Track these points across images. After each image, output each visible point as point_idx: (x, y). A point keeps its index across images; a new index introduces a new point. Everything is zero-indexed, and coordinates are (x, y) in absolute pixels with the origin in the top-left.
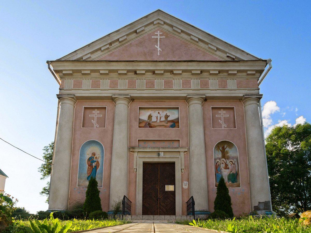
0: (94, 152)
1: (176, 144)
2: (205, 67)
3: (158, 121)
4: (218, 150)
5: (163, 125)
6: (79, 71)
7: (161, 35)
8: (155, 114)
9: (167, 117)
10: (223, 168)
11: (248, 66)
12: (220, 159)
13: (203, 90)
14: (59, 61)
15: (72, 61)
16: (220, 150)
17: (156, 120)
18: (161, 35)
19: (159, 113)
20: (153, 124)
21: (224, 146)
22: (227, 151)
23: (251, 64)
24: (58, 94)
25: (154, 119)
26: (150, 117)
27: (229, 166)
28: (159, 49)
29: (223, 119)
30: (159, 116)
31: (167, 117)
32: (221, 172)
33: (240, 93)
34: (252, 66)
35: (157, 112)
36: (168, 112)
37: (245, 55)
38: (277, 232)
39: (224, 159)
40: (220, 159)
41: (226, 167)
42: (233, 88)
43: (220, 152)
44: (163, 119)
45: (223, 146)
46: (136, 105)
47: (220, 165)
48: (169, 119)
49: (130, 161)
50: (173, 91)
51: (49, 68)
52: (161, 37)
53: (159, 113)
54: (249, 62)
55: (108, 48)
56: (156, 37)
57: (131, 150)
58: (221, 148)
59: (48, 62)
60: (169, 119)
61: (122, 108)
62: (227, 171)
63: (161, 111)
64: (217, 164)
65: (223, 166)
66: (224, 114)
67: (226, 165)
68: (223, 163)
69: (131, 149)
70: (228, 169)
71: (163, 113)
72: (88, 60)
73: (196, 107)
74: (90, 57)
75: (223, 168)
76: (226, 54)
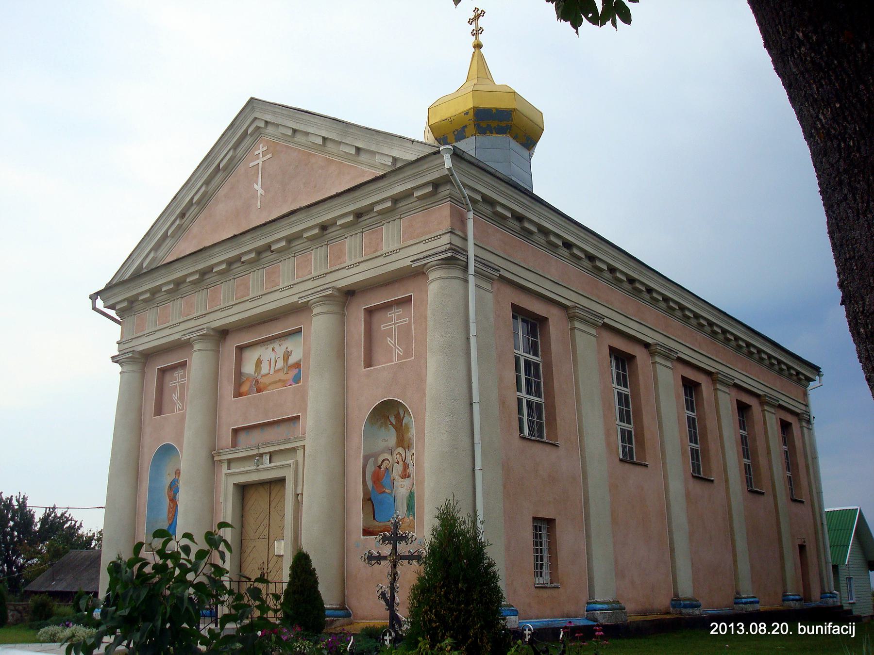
0: (538, 451)
2: (325, 216)
3: (272, 372)
4: (386, 426)
5: (280, 380)
8: (266, 354)
9: (287, 355)
10: (397, 478)
11: (404, 180)
12: (391, 451)
13: (338, 270)
14: (109, 287)
16: (392, 424)
18: (265, 153)
19: (273, 350)
21: (399, 413)
23: (414, 171)
25: (265, 369)
26: (259, 362)
27: (412, 470)
28: (261, 191)
29: (395, 335)
30: (273, 355)
31: (287, 355)
32: (392, 487)
33: (403, 261)
35: (270, 347)
36: (289, 344)
37: (409, 145)
39: (400, 450)
40: (391, 451)
41: (405, 475)
43: (393, 431)
44: (280, 364)
45: (388, 413)
46: (230, 347)
47: (390, 470)
48: (292, 360)
53: (273, 350)
54: (405, 169)
58: (393, 419)
59: (483, 12)
61: (198, 361)
62: (407, 482)
63: (276, 345)
64: (380, 467)
65: (398, 469)
67: (406, 466)
68: (398, 463)
69: (213, 461)
70: (409, 477)
71: (280, 348)
72: (153, 266)
73: (320, 325)
74: (154, 259)
75: (397, 478)
76: (137, 300)
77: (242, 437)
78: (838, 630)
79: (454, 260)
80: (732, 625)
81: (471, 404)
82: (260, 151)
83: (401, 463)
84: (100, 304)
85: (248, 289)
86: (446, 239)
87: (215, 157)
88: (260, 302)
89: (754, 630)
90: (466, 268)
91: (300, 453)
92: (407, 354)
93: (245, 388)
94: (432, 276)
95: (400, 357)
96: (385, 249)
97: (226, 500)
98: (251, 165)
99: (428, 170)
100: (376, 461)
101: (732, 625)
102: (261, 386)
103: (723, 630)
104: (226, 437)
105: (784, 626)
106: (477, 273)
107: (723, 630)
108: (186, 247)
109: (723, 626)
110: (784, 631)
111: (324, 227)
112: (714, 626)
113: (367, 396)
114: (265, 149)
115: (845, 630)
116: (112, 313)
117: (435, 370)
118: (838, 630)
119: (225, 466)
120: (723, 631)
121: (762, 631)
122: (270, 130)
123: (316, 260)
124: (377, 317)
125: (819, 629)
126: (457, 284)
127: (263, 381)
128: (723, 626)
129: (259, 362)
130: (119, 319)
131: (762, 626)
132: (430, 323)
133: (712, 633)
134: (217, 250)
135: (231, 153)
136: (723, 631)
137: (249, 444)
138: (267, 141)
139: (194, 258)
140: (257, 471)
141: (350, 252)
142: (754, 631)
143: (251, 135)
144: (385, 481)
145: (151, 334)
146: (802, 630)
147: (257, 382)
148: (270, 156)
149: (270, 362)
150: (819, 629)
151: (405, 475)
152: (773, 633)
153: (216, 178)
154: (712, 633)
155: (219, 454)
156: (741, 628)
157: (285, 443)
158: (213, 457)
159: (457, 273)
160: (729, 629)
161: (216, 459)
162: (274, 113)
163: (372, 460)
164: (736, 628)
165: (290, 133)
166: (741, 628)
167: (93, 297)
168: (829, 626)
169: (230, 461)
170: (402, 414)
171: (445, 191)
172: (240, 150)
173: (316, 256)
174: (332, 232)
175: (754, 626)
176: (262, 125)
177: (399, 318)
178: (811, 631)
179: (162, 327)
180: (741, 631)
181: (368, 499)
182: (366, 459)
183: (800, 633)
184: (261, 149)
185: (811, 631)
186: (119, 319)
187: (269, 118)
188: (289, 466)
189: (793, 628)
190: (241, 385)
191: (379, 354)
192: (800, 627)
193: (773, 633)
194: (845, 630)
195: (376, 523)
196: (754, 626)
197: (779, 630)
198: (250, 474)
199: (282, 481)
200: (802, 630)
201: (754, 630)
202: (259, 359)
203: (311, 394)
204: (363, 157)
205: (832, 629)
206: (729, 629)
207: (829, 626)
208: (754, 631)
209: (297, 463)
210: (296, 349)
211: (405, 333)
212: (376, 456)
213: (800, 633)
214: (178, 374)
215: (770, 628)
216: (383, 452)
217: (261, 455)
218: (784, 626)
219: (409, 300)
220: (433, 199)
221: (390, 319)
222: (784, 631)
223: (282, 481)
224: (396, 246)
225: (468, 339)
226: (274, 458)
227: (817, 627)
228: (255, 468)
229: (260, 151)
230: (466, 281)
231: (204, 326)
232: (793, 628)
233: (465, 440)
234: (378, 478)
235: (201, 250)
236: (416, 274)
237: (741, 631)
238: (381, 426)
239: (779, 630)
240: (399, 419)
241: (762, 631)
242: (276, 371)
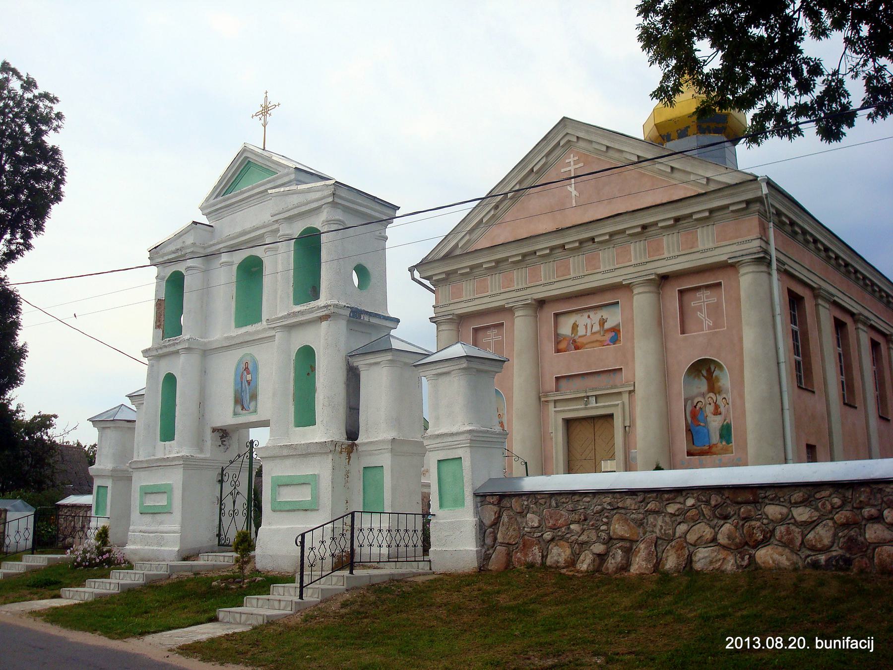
1: (601, 384)
3: (589, 334)
5: (597, 341)
6: (455, 271)
7: (576, 163)
8: (582, 320)
9: (602, 322)
11: (726, 196)
12: (703, 395)
15: (438, 260)
17: (584, 333)
18: (576, 163)
19: (589, 317)
20: (580, 340)
21: (710, 368)
22: (716, 377)
24: (434, 315)
25: (581, 331)
26: (575, 327)
27: (722, 409)
28: (574, 193)
29: (705, 310)
30: (588, 321)
31: (602, 322)
32: (706, 421)
33: (721, 256)
34: (732, 194)
35: (586, 315)
36: (604, 313)
38: (290, 668)
39: (711, 395)
40: (703, 395)
41: (717, 412)
42: (707, 247)
43: (704, 381)
44: (596, 328)
45: (704, 369)
46: (548, 313)
48: (607, 326)
49: (541, 422)
50: (599, 276)
51: (414, 279)
52: (577, 166)
53: (589, 317)
55: (493, 216)
56: (568, 169)
57: (543, 399)
58: (704, 372)
60: (607, 326)
61: (520, 326)
62: (719, 418)
63: (592, 314)
65: (710, 409)
66: (707, 297)
67: (717, 407)
69: (542, 400)
70: (720, 414)
71: (596, 316)
73: (642, 302)
75: (709, 415)
77: (563, 383)
78: (856, 645)
79: (763, 260)
80: (748, 639)
81: (778, 363)
82: (571, 160)
83: (713, 404)
84: (417, 275)
85: (569, 270)
86: (757, 243)
87: (530, 161)
88: (583, 281)
89: (770, 645)
90: (769, 264)
91: (626, 397)
92: (716, 325)
93: (563, 346)
94: (743, 270)
95: (709, 328)
96: (701, 247)
97: (556, 429)
98: (562, 170)
99: (743, 192)
100: (692, 403)
101: (748, 639)
102: (579, 344)
103: (739, 645)
104: (551, 384)
105: (801, 640)
106: (778, 270)
107: (739, 645)
108: (501, 234)
109: (739, 640)
110: (801, 645)
111: (644, 227)
112: (730, 640)
113: (687, 352)
114: (576, 158)
115: (863, 644)
116: (427, 283)
117: (751, 338)
118: (856, 645)
119: (551, 405)
120: (739, 645)
121: (779, 645)
122: (581, 144)
123: (636, 251)
124: (686, 297)
125: (837, 643)
126: (764, 276)
127: (580, 341)
128: (739, 640)
129: (575, 327)
130: (432, 287)
131: (779, 640)
132: (745, 306)
133: (727, 647)
134: (542, 238)
135: (544, 160)
136: (739, 645)
137: (570, 390)
138: (578, 153)
139: (519, 243)
140: (586, 409)
141: (668, 247)
142: (770, 645)
143: (563, 146)
144: (700, 417)
145: (470, 300)
146: (819, 644)
147: (574, 341)
148: (581, 165)
149: (586, 326)
150: (837, 643)
151: (717, 412)
152: (790, 647)
153: (529, 178)
154: (727, 647)
155: (546, 396)
156: (758, 642)
157: (612, 388)
158: (540, 398)
159: (763, 268)
160: (745, 643)
161: (543, 399)
162: (587, 132)
163: (689, 402)
164: (752, 643)
165: (604, 149)
166: (758, 642)
167: (411, 270)
168: (848, 641)
169: (555, 401)
170: (713, 369)
171: (756, 207)
172: (552, 158)
173: (635, 248)
174: (652, 231)
175: (770, 640)
176: (575, 139)
177: (707, 297)
178: (828, 645)
179: (472, 297)
180: (757, 645)
181: (689, 430)
182: (686, 400)
183: (817, 647)
184: (572, 159)
185: (828, 645)
186: (432, 287)
187: (581, 135)
188: (618, 405)
189: (811, 642)
190: (560, 344)
191: (690, 324)
192: (817, 641)
193: (790, 647)
194: (863, 644)
195: (694, 447)
196: (770, 640)
197: (796, 645)
198: (578, 411)
199: (611, 416)
200: (819, 644)
201: (770, 645)
202: (574, 324)
203: (638, 353)
204: (676, 175)
205: (850, 644)
206: (745, 643)
207: (848, 641)
208: (770, 645)
209: (623, 403)
210: (613, 318)
211: (715, 310)
212: (692, 399)
213: (817, 647)
214: (492, 333)
215: (786, 643)
216: (697, 396)
217: (588, 397)
218: (801, 640)
219: (719, 284)
220: (744, 212)
221: (700, 299)
222: (801, 645)
223: (611, 416)
224: (711, 245)
225: (774, 316)
226: (599, 400)
227: (835, 641)
228: (583, 406)
229: (571, 160)
230: (770, 274)
231: (529, 297)
232: (811, 642)
233: (777, 388)
234: (694, 415)
235: (531, 237)
236: (729, 267)
237: (757, 645)
238: (695, 377)
239: (796, 645)
240: (710, 373)
241: (779, 645)
242: (593, 334)
